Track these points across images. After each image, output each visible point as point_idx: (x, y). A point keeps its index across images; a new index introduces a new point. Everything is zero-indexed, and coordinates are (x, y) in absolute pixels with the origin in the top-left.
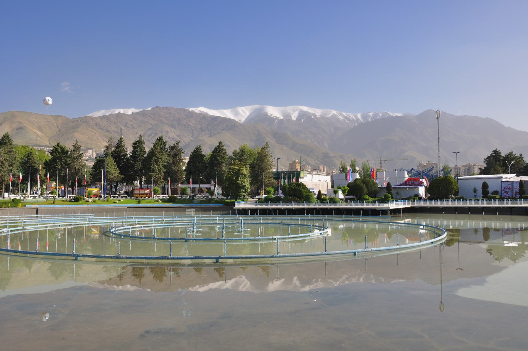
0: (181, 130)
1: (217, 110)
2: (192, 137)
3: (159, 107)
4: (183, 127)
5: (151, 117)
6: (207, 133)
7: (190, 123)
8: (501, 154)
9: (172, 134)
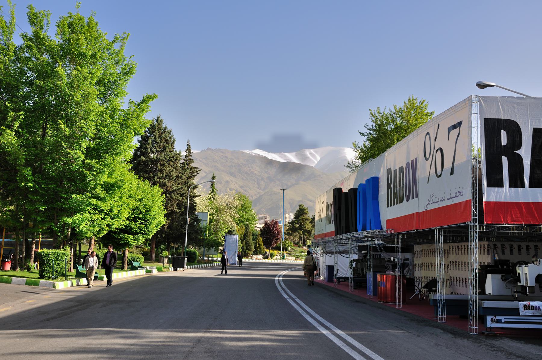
0: (243, 179)
1: (278, 154)
2: (258, 188)
3: (211, 149)
4: (245, 176)
5: (203, 162)
6: (278, 184)
7: (254, 171)
8: (304, 207)
9: (234, 184)
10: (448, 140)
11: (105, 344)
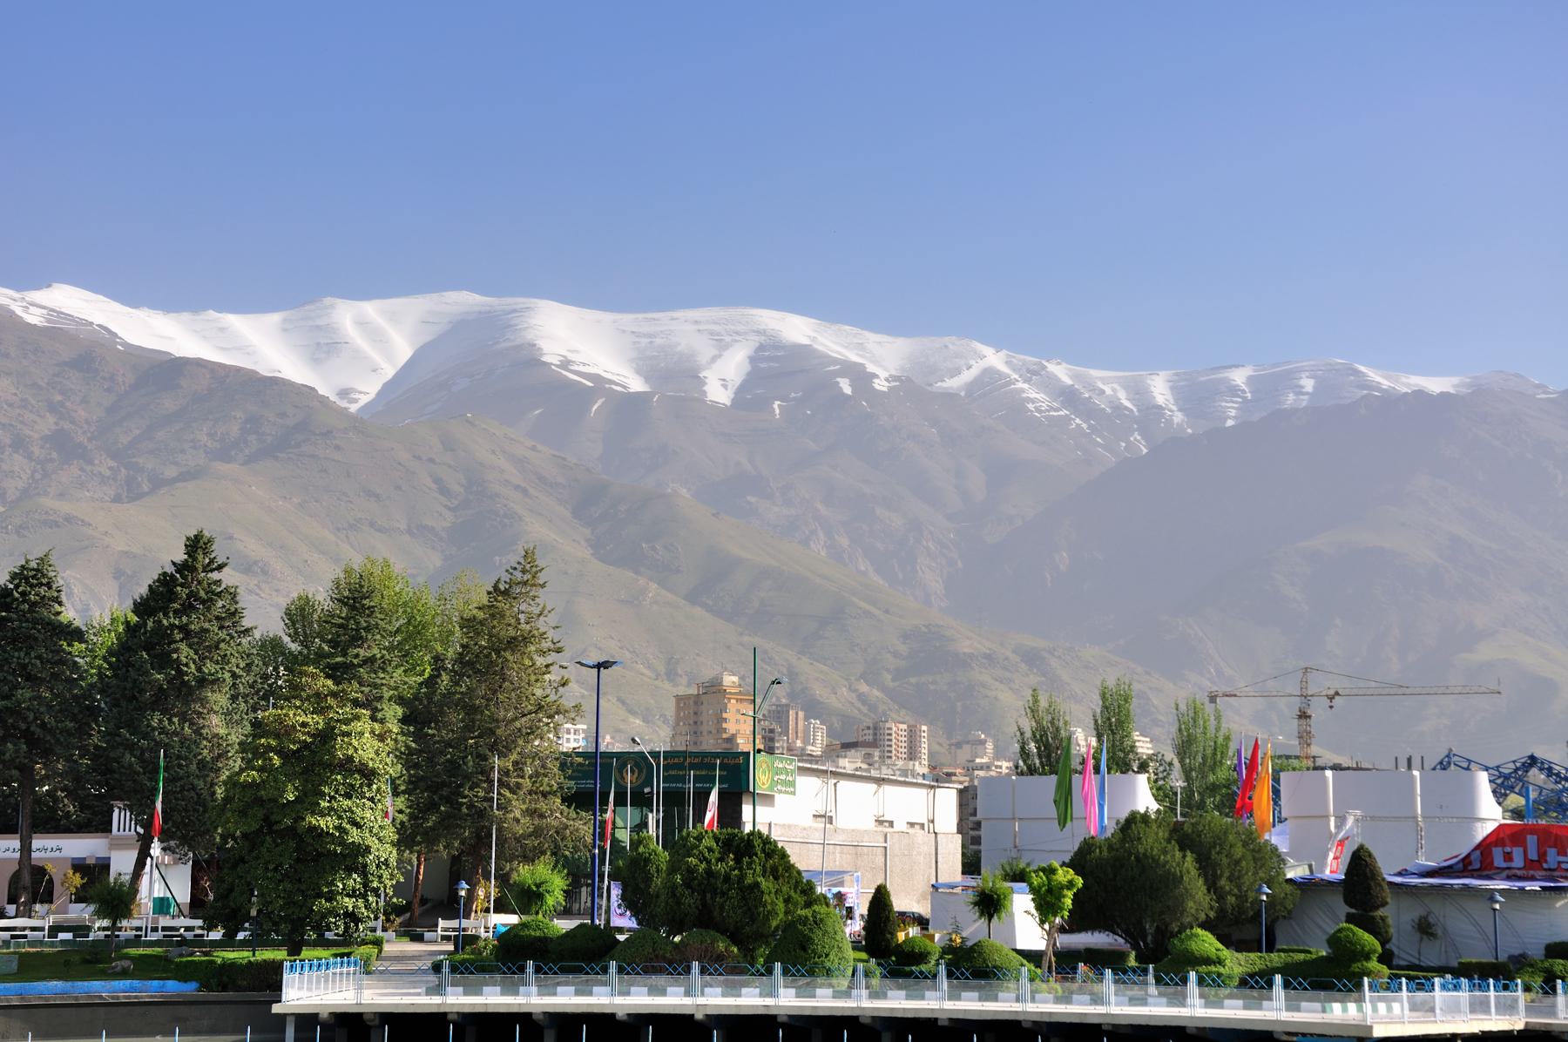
1: (186, 316)
6: (108, 473)
10: (1396, 759)
11: (1138, 999)
